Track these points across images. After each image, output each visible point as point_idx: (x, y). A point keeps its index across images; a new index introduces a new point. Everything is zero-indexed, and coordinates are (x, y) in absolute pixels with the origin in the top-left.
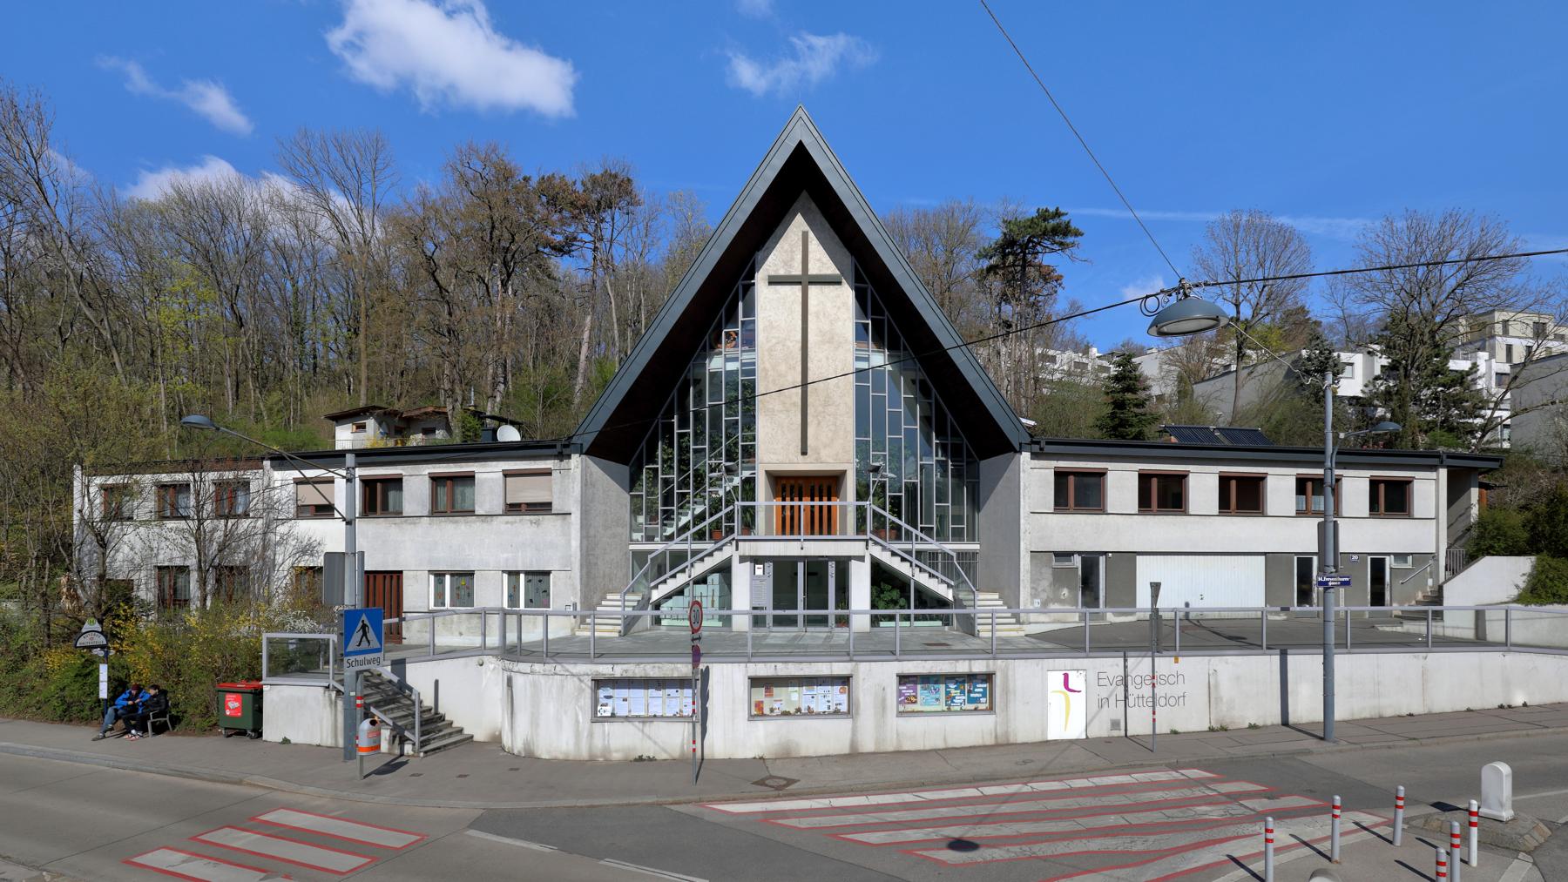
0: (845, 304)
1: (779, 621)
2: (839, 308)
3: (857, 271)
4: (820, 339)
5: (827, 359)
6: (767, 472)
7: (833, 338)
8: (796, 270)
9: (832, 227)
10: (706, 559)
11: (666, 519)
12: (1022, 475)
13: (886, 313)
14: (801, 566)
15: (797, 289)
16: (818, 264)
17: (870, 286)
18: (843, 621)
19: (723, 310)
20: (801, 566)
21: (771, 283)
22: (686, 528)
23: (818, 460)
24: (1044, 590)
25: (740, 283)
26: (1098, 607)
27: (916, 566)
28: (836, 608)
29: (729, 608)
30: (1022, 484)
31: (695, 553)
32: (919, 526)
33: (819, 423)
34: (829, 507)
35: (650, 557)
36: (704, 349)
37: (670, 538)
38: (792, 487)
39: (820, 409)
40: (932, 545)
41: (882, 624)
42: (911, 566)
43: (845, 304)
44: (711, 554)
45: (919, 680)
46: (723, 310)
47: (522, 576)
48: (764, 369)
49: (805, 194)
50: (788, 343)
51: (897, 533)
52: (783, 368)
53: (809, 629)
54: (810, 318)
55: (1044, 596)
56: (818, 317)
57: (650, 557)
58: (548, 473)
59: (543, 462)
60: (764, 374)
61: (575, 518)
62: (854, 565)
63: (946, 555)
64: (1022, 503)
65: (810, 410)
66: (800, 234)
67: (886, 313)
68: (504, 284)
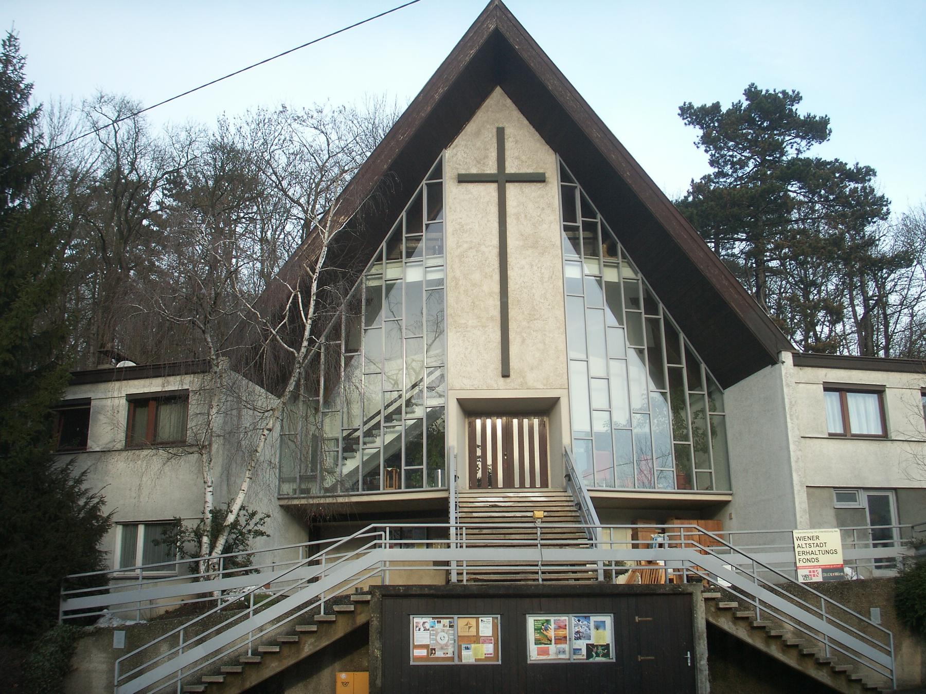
0: (549, 205)
2: (543, 209)
3: (561, 164)
4: (521, 243)
5: (532, 266)
6: (461, 402)
7: (537, 242)
8: (512, 190)
9: (530, 123)
12: (785, 390)
13: (599, 216)
17: (578, 185)
19: (404, 214)
21: (460, 182)
23: (524, 385)
25: (424, 182)
29: (686, 547)
30: (787, 401)
33: (523, 341)
36: (380, 258)
39: (524, 323)
46: (404, 214)
47: (141, 529)
48: (454, 277)
49: (498, 91)
50: (483, 248)
52: (477, 276)
54: (509, 220)
56: (518, 219)
59: (142, 382)
60: (453, 284)
64: (789, 425)
65: (512, 326)
66: (495, 130)
67: (661, 306)
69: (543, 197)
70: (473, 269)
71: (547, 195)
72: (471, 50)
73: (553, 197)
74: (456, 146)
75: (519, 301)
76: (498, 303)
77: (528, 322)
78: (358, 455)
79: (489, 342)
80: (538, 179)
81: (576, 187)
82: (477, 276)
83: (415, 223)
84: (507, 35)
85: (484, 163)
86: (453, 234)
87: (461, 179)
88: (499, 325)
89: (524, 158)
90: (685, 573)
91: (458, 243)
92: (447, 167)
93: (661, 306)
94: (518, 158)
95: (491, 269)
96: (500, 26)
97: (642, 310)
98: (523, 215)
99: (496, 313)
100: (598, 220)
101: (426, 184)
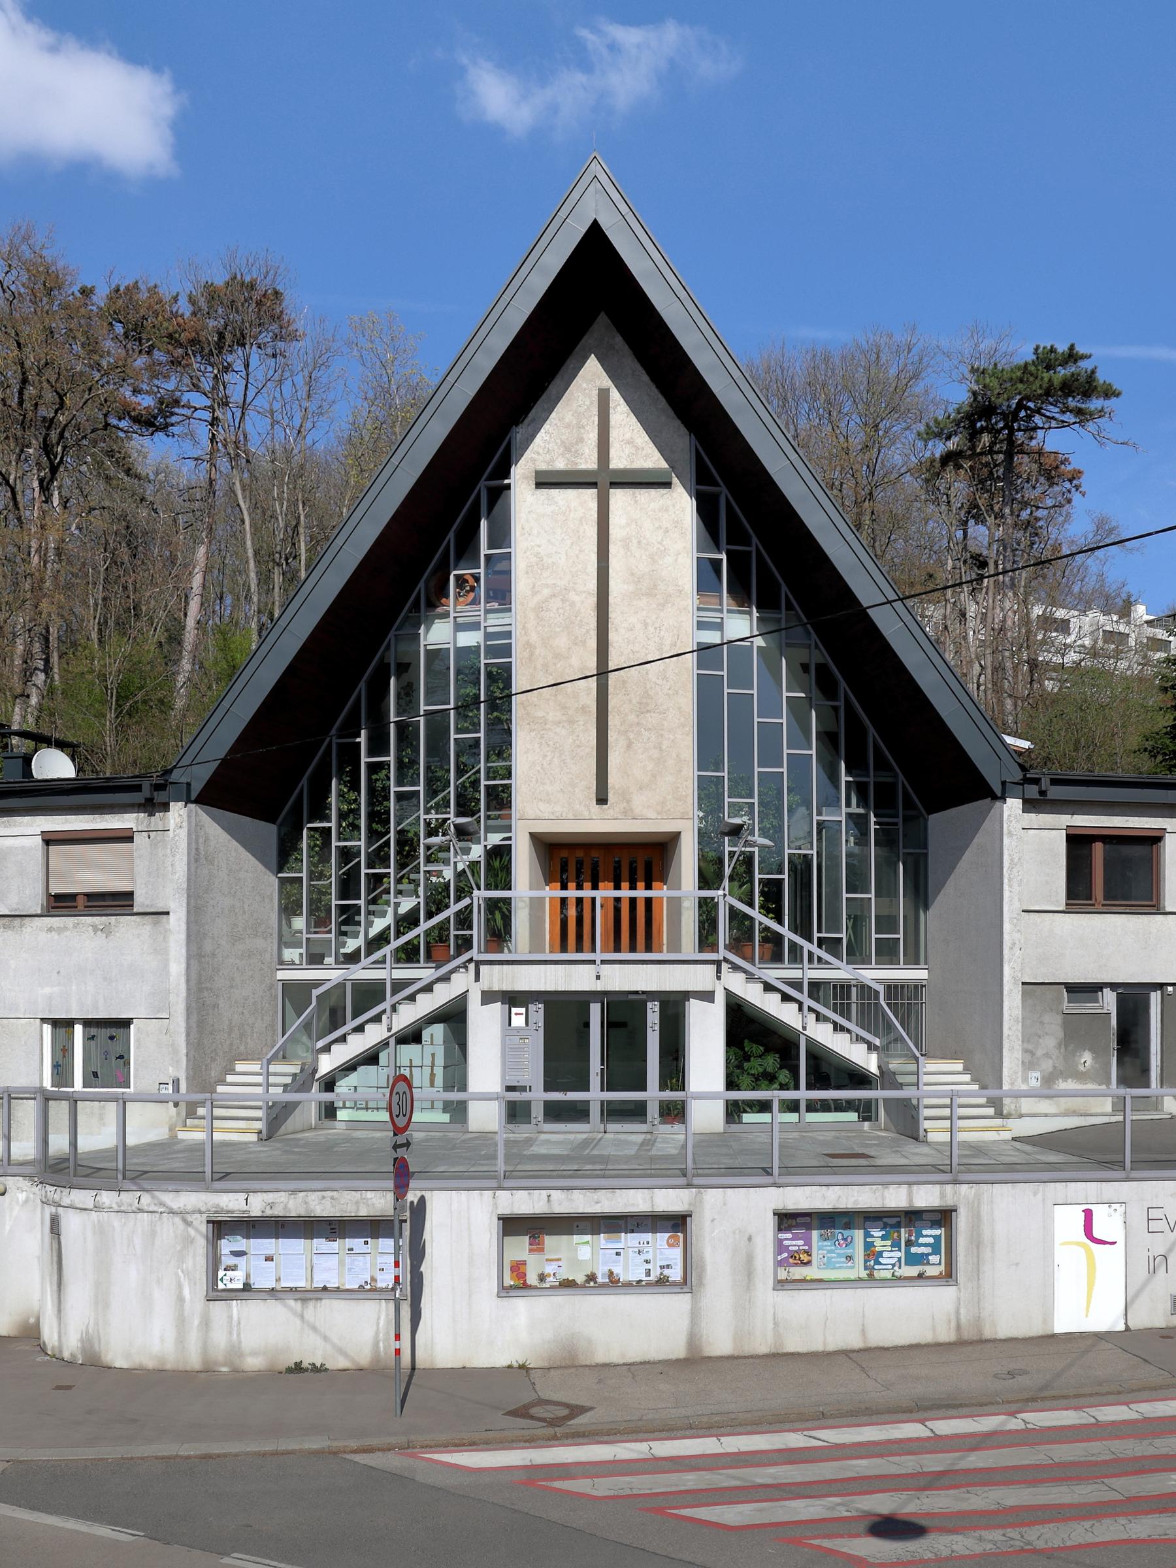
1: (555, 1112)
2: (667, 531)
5: (646, 625)
11: (345, 923)
13: (755, 540)
14: (595, 1010)
16: (628, 450)
18: (674, 1112)
20: (595, 1010)
22: (382, 939)
26: (1147, 1086)
27: (811, 1009)
29: (463, 1087)
31: (398, 986)
32: (816, 935)
35: (316, 993)
36: (416, 606)
38: (580, 864)
39: (632, 718)
40: (840, 971)
41: (747, 1118)
42: (801, 1009)
43: (677, 523)
44: (428, 988)
46: (451, 535)
47: (78, 1029)
57: (316, 993)
58: (126, 837)
61: (177, 922)
62: (694, 1007)
69: (667, 510)
70: (558, 630)
71: (674, 506)
73: (683, 511)
74: (533, 420)
77: (638, 716)
79: (579, 746)
85: (576, 451)
86: (527, 573)
91: (534, 587)
93: (843, 685)
95: (584, 631)
98: (635, 541)
100: (753, 549)
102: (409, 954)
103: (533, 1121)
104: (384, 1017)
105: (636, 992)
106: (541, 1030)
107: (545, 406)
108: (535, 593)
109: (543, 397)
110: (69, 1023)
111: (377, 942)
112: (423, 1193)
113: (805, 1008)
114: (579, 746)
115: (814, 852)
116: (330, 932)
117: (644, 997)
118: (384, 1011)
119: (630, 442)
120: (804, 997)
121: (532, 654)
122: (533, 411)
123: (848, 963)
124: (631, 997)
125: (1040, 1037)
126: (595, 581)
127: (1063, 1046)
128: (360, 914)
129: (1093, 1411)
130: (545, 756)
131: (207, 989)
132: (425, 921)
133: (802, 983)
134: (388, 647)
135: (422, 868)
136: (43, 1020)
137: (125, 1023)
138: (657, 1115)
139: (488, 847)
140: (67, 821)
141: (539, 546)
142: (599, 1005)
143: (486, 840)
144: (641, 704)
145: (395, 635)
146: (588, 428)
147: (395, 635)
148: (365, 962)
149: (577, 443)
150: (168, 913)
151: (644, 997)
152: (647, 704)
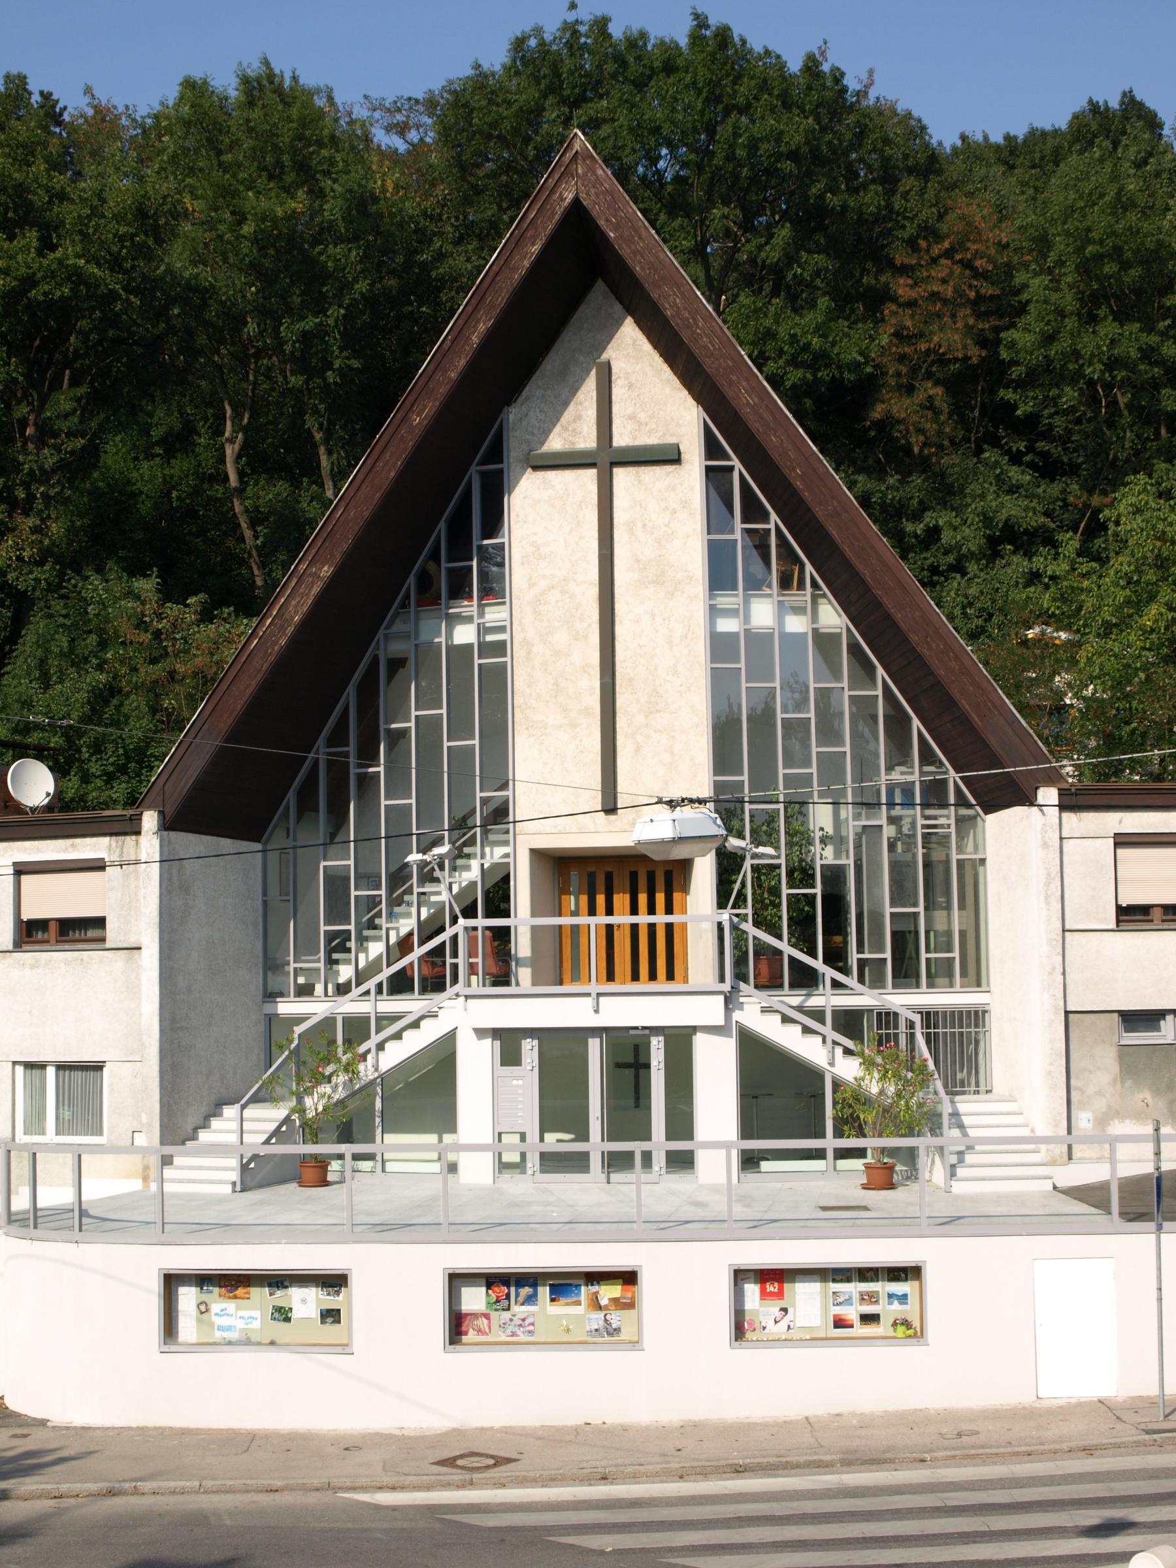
1: (553, 1162)
2: (674, 512)
5: (653, 616)
8: (622, 477)
10: (405, 1034)
11: (336, 949)
13: (774, 516)
14: (594, 1046)
15: (588, 479)
16: (630, 426)
17: (736, 463)
18: (682, 1161)
19: (442, 526)
20: (594, 1046)
22: (374, 967)
24: (1100, 1093)
25: (474, 470)
26: (43, 1133)
27: (835, 1043)
28: (57, 1134)
29: (689, 1134)
31: (385, 1020)
32: (854, 957)
33: (638, 749)
34: (669, 927)
35: (299, 1030)
36: (404, 605)
37: (343, 989)
38: (609, 878)
39: (640, 719)
40: (862, 998)
41: (765, 1165)
42: (824, 1041)
43: (685, 504)
44: (415, 1025)
45: (855, 1276)
46: (442, 526)
47: (51, 1071)
51: (805, 978)
53: (614, 1177)
55: (1101, 1104)
57: (299, 1030)
58: (98, 866)
61: (150, 957)
62: (701, 1042)
63: (888, 1018)
68: (911, 190)
69: (674, 489)
70: (557, 624)
71: (681, 484)
72: (533, 244)
73: (692, 489)
74: (527, 399)
75: (630, 680)
76: (597, 684)
77: (646, 717)
78: (475, 864)
79: (582, 752)
80: (669, 457)
81: (731, 469)
82: (561, 638)
83: (461, 546)
84: (595, 211)
85: (574, 430)
86: (523, 563)
87: (91, 1074)
88: (599, 723)
89: (642, 416)
90: (830, 1142)
91: (530, 579)
92: (511, 440)
93: (880, 672)
94: (632, 417)
95: (586, 625)
96: (582, 196)
97: (845, 684)
98: (639, 525)
99: (594, 701)
100: (772, 526)
101: (477, 471)
102: (400, 984)
103: (530, 1172)
104: (369, 1057)
105: (636, 1028)
106: (536, 1070)
107: (540, 384)
108: (532, 585)
109: (538, 373)
110: (42, 1066)
111: (361, 977)
112: (893, 1334)
113: (829, 1041)
114: (582, 752)
115: (851, 862)
116: (318, 961)
117: (647, 1032)
118: (369, 1051)
119: (632, 417)
120: (827, 1029)
121: (529, 652)
122: (527, 389)
123: (871, 987)
124: (632, 1032)
125: (1090, 1072)
126: (597, 570)
127: (1118, 1083)
128: (350, 940)
129: (1012, 1467)
130: (545, 764)
131: (182, 1029)
132: (419, 946)
133: (823, 1012)
134: (377, 647)
135: (416, 890)
136: (15, 1063)
137: (98, 1067)
138: (663, 1163)
139: (486, 866)
140: (39, 850)
141: (535, 534)
142: (598, 1040)
143: (483, 856)
144: (649, 703)
145: (385, 635)
146: (586, 404)
147: (385, 635)
148: (356, 992)
149: (574, 421)
150: (140, 948)
151: (647, 1032)
152: (657, 703)
